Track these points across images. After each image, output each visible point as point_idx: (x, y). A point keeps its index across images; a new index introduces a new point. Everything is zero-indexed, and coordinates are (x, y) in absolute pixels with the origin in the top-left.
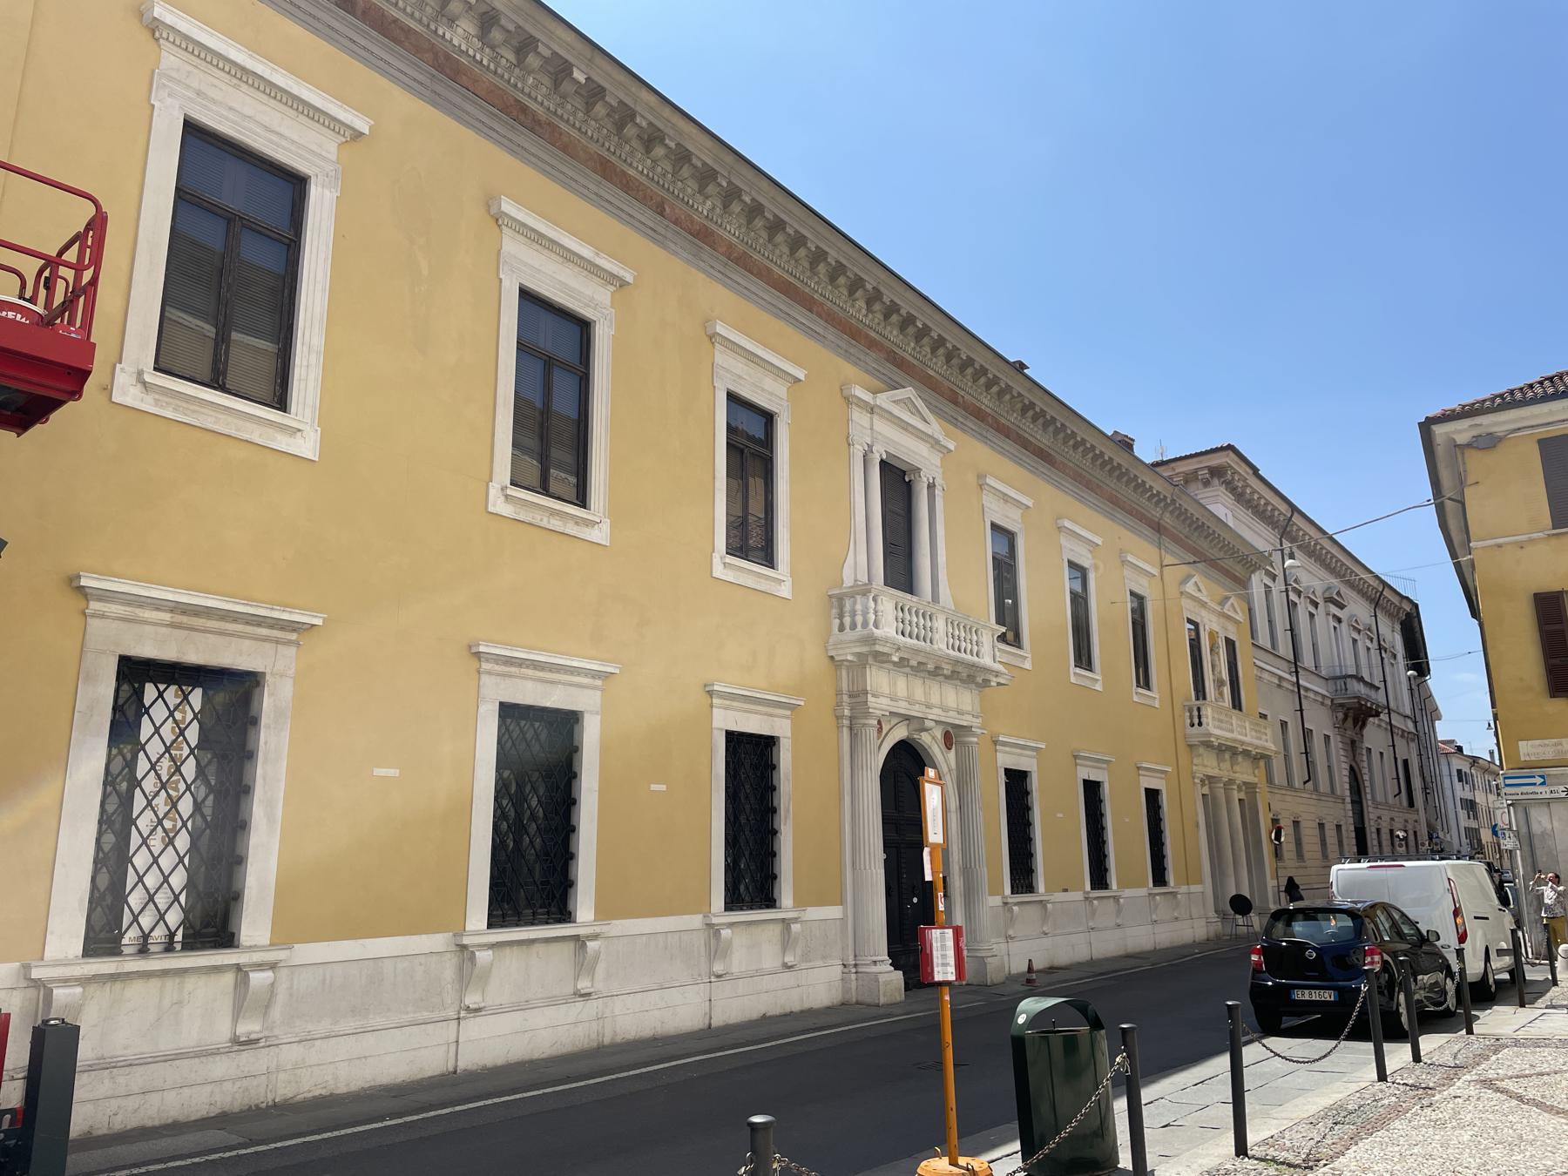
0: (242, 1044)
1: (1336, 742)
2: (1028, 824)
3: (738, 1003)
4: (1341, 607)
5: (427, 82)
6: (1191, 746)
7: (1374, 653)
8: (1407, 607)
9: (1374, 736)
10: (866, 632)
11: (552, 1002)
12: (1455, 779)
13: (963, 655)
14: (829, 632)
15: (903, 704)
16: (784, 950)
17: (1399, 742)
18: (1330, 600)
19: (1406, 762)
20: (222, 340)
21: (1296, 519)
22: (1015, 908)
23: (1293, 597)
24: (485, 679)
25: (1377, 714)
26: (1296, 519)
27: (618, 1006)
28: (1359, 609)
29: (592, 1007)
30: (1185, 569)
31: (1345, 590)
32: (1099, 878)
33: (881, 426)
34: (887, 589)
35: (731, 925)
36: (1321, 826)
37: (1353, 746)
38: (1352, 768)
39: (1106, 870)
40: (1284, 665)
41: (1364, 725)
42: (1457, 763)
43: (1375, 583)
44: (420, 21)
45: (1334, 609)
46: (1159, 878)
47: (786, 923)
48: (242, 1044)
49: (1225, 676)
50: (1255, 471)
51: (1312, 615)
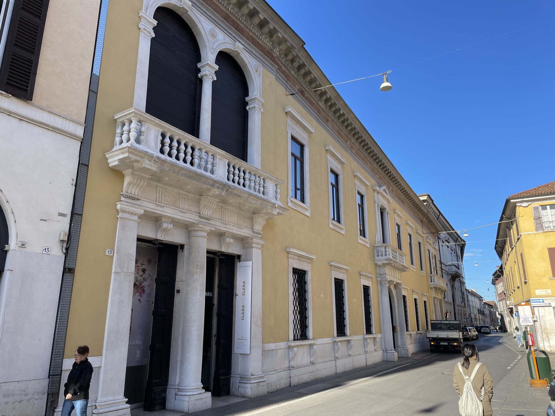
0: (312, 363)
4: (449, 243)
6: (431, 288)
10: (386, 257)
14: (374, 257)
16: (375, 346)
18: (446, 241)
21: (441, 216)
22: (339, 343)
24: (290, 259)
26: (441, 216)
30: (428, 235)
31: (450, 239)
32: (341, 331)
33: (380, 197)
34: (148, 116)
35: (298, 346)
37: (453, 287)
39: (345, 326)
44: (245, 25)
45: (447, 244)
46: (369, 330)
50: (433, 201)
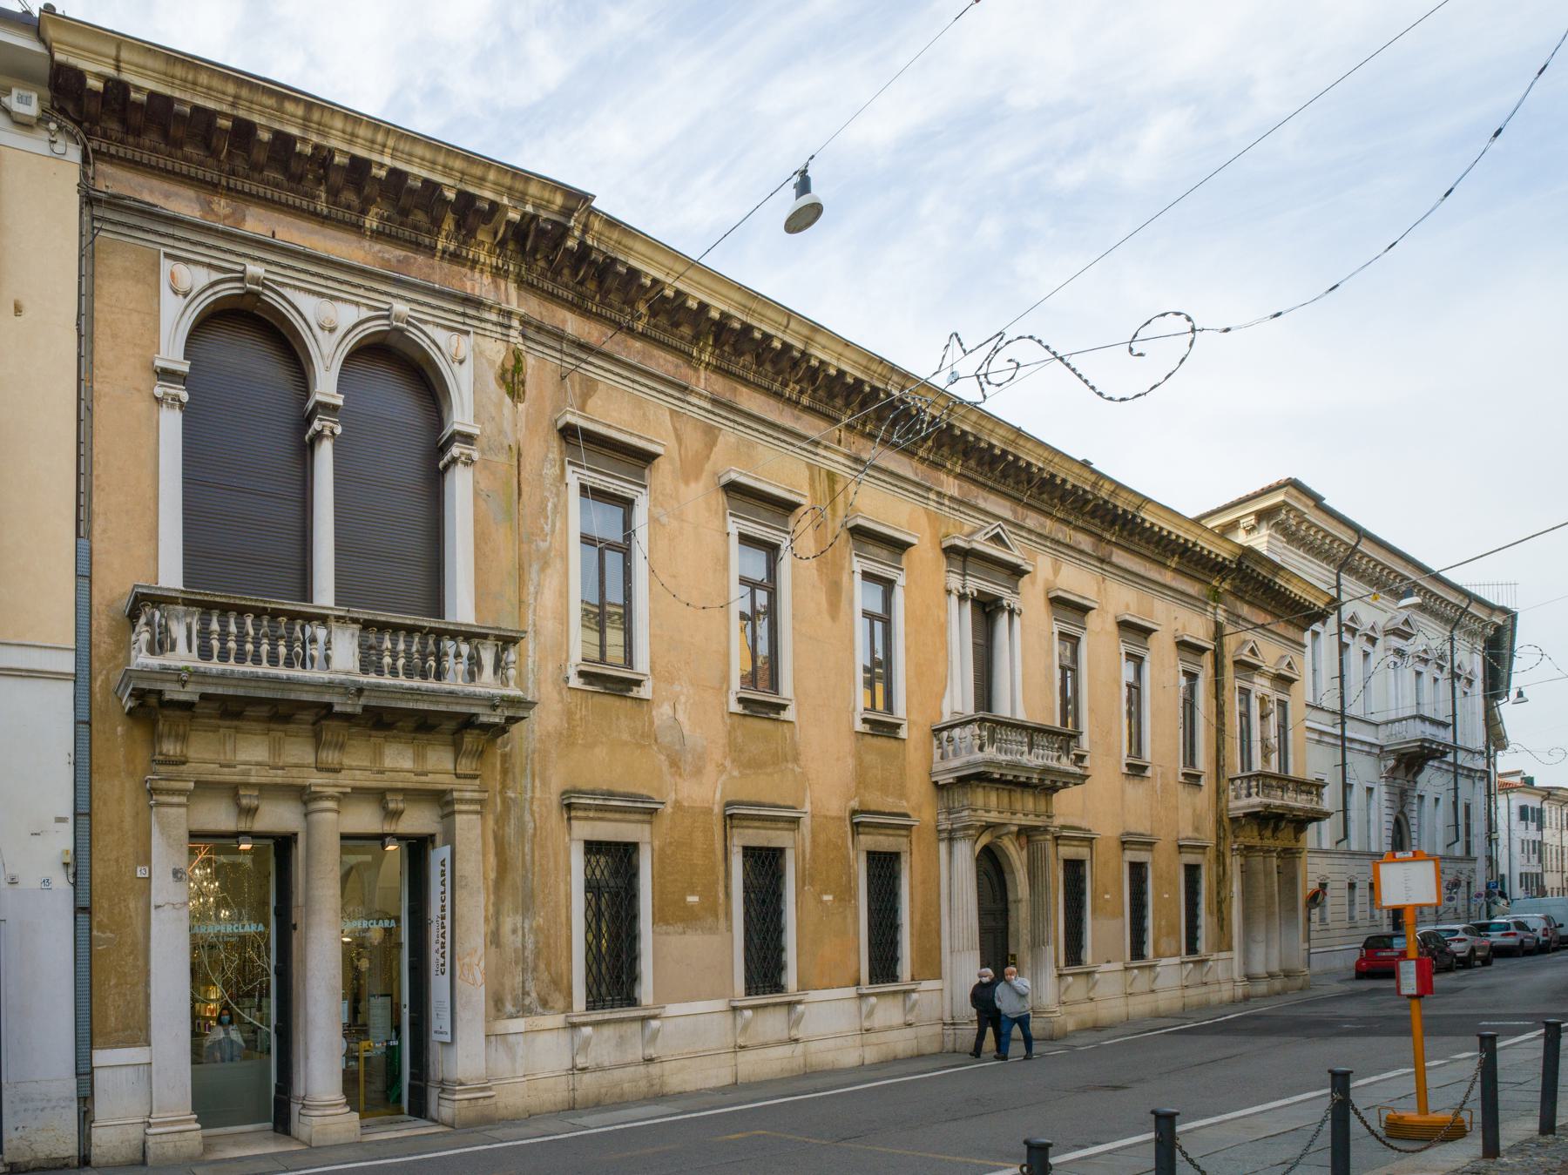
1: (1381, 793)
2: (983, 913)
3: (1140, 1006)
5: (709, 407)
7: (1444, 685)
8: (1498, 619)
9: (1432, 781)
11: (780, 1043)
12: (1515, 817)
13: (248, 668)
15: (994, 814)
17: (1464, 783)
19: (1467, 807)
20: (602, 633)
21: (1365, 547)
23: (1347, 638)
25: (1444, 754)
27: (813, 1046)
28: (1430, 635)
29: (800, 1048)
36: (1352, 886)
38: (1397, 821)
40: (1327, 718)
41: (1421, 770)
42: (1517, 800)
43: (1347, 536)
45: (1396, 642)
47: (906, 993)
48: (649, 1060)
49: (1274, 741)
50: (1317, 501)
51: (1366, 655)
